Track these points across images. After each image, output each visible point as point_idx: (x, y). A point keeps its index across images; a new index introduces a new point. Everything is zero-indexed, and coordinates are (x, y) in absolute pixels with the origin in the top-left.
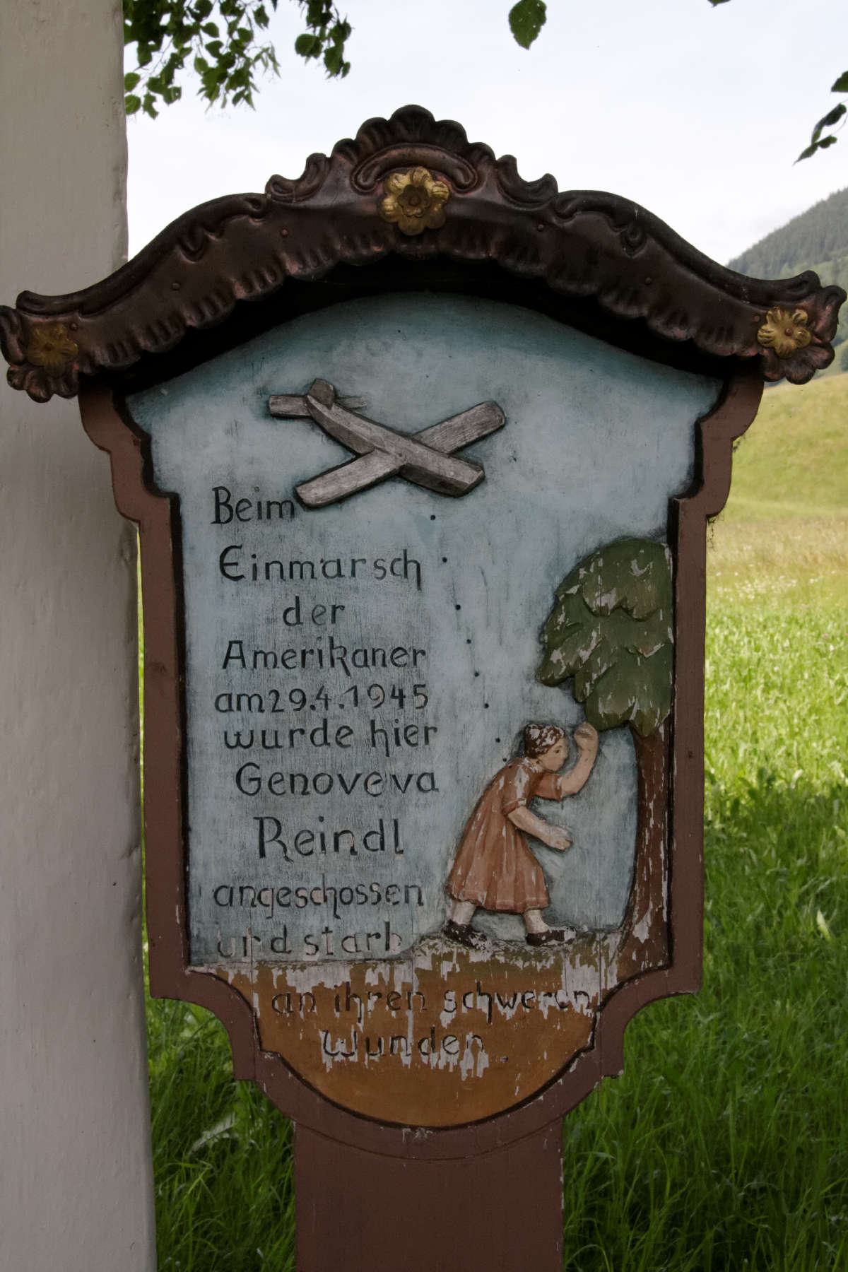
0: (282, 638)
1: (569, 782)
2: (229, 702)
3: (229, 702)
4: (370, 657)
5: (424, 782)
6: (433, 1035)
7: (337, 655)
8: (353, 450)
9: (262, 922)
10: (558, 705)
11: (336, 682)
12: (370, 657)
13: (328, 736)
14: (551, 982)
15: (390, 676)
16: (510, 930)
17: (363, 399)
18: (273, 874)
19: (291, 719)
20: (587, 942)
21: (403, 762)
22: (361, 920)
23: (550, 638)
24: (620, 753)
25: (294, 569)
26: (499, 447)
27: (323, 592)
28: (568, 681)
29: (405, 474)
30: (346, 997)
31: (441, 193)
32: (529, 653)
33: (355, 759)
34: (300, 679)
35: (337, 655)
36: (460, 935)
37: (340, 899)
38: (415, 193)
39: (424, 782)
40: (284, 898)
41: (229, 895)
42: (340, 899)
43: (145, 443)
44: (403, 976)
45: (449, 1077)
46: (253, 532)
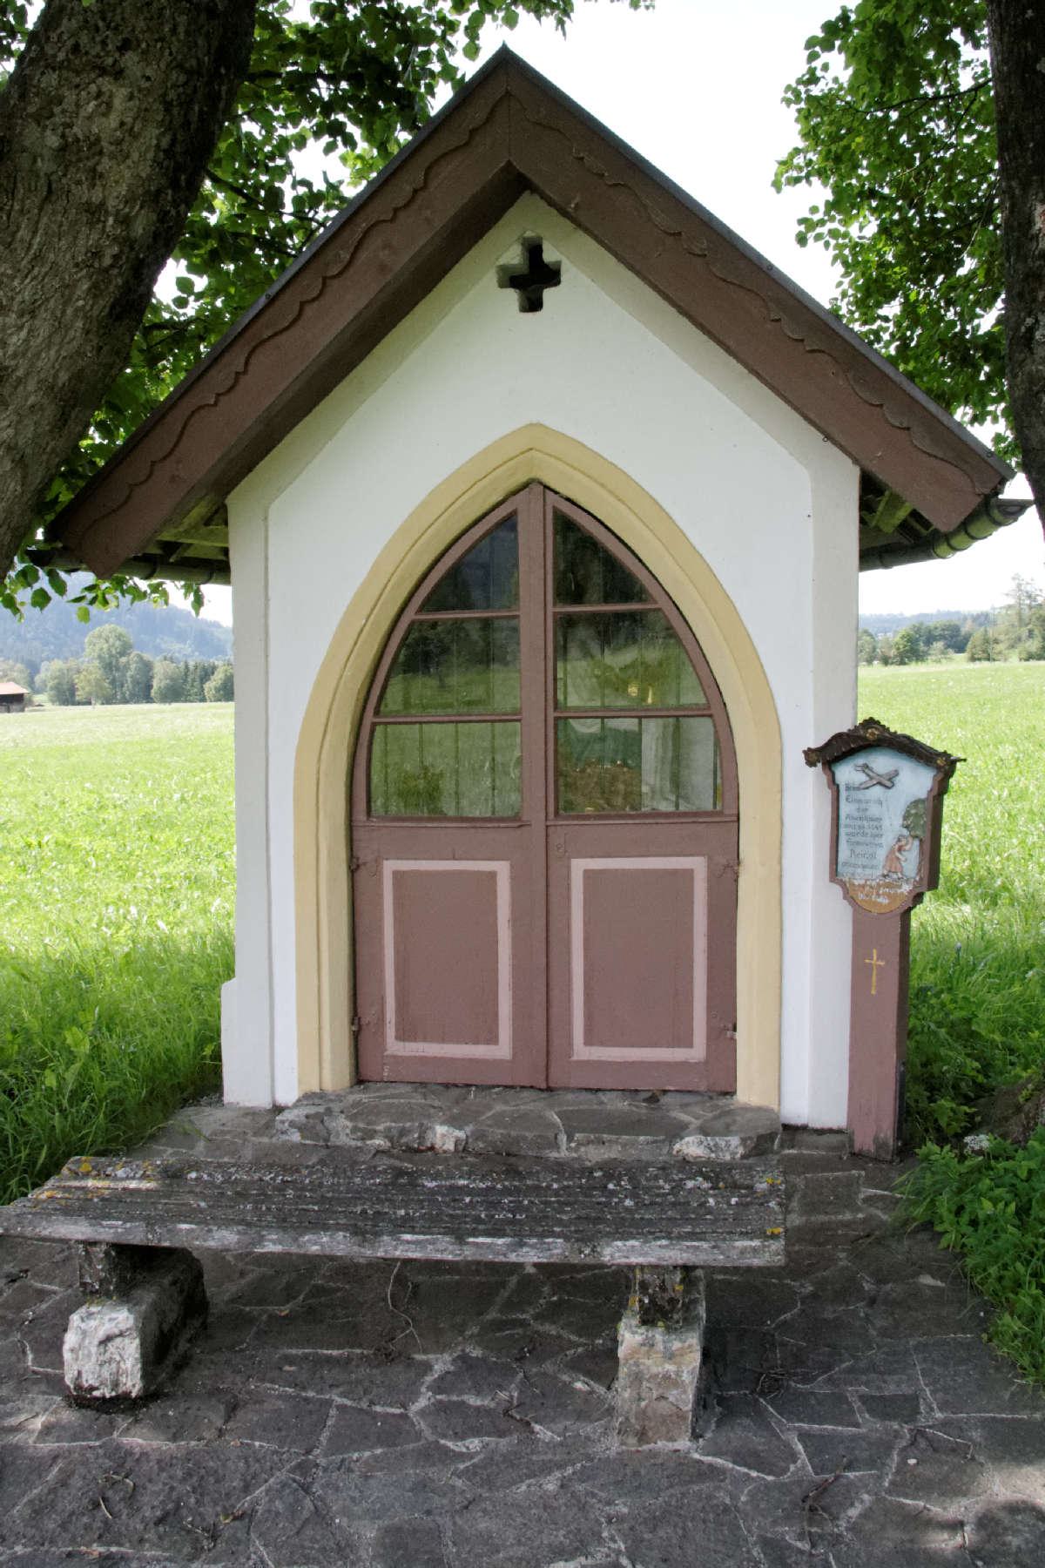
0: (856, 814)
1: (907, 847)
2: (847, 826)
3: (847, 826)
4: (872, 820)
5: (880, 845)
6: (878, 895)
7: (866, 819)
8: (871, 778)
9: (851, 870)
10: (905, 832)
11: (865, 823)
12: (872, 820)
13: (865, 834)
14: (900, 887)
15: (875, 823)
16: (895, 876)
17: (78, 1040)
18: (853, 861)
19: (857, 831)
20: (907, 881)
21: (877, 841)
22: (868, 871)
23: (905, 818)
24: (917, 843)
25: (860, 801)
26: (898, 778)
27: (863, 806)
28: (907, 827)
29: (880, 783)
30: (863, 886)
31: (120, 1173)
32: (900, 821)
33: (868, 839)
34: (859, 823)
35: (866, 819)
36: (885, 876)
37: (864, 867)
38: (873, 734)
39: (880, 845)
40: (855, 866)
41: (845, 864)
42: (864, 867)
43: (833, 774)
44: (874, 883)
45: (881, 904)
46: (852, 792)
